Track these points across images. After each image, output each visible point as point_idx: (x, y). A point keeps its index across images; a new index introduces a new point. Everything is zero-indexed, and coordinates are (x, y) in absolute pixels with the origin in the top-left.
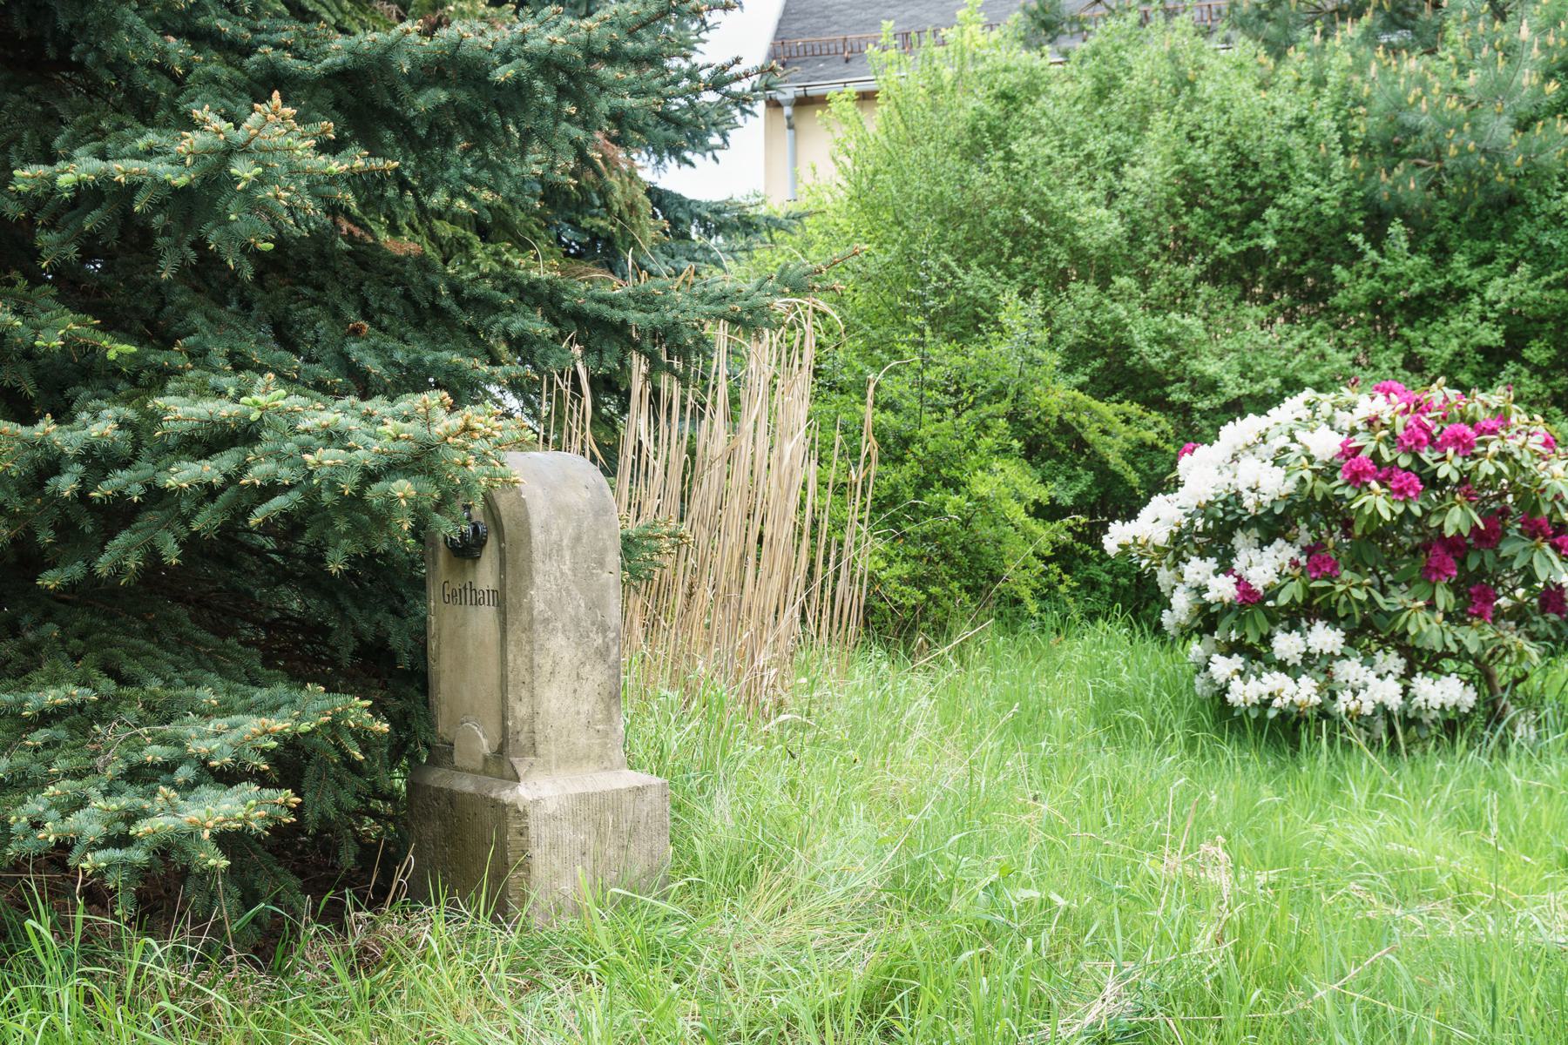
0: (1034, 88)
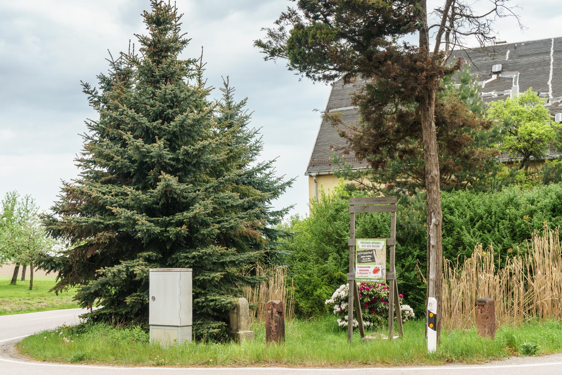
0: (343, 207)
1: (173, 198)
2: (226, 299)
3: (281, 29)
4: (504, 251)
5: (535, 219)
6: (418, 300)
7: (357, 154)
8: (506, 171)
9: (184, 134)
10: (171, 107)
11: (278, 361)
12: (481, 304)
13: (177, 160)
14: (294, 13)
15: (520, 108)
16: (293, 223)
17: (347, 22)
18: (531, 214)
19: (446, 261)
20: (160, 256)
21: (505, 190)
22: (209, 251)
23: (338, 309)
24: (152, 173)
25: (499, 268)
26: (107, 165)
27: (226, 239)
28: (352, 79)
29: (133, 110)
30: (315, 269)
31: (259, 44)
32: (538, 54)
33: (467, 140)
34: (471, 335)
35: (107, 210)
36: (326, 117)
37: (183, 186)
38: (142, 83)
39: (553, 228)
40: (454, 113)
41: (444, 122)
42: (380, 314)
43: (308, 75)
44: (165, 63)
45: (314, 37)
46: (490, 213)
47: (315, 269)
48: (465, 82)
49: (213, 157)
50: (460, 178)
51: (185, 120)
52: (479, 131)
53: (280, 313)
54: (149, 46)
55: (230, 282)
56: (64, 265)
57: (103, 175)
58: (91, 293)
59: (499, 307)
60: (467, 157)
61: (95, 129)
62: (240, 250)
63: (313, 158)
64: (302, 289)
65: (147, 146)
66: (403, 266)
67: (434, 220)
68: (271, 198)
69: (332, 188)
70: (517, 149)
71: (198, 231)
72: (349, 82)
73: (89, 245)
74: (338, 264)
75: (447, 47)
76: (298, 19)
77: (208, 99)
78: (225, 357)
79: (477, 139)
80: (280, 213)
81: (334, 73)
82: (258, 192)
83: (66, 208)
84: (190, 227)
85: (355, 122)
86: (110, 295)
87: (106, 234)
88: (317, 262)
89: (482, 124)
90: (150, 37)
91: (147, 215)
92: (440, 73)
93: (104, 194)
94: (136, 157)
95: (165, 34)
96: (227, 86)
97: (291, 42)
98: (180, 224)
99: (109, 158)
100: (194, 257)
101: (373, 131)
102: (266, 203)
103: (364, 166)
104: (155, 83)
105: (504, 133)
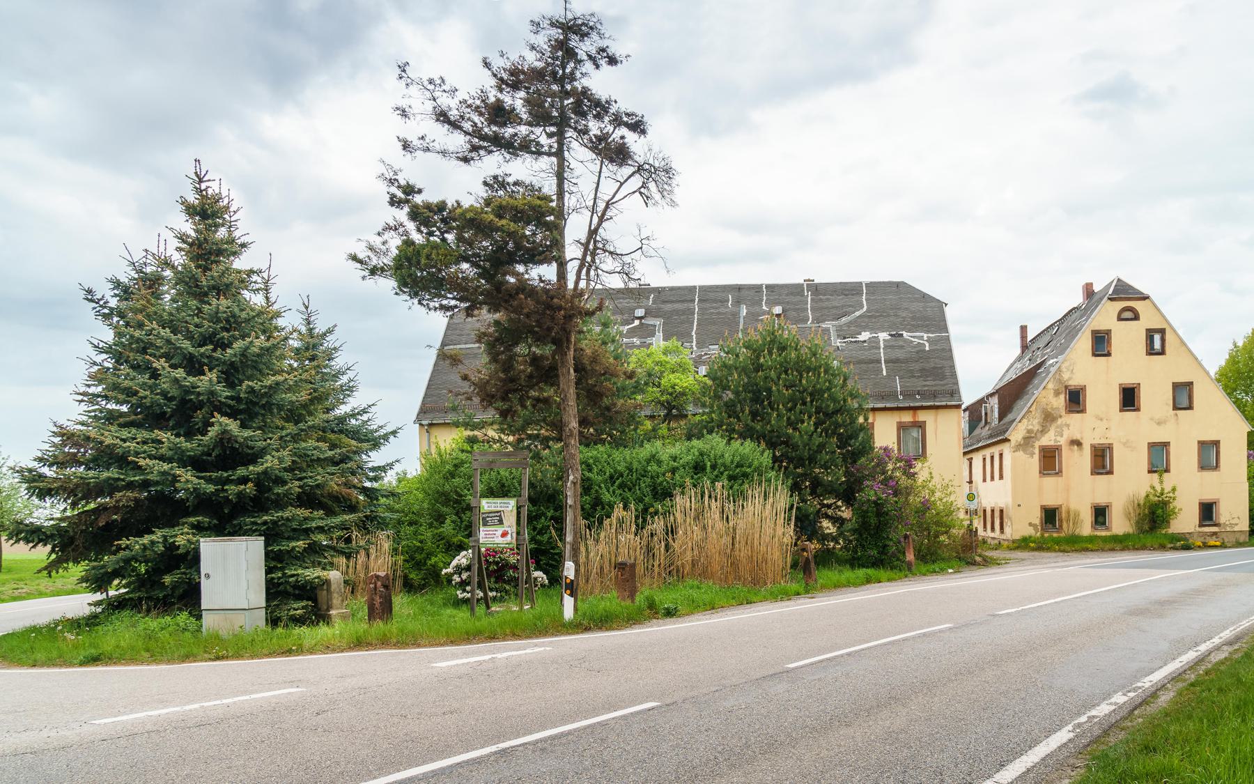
0: (463, 462)
1: (233, 448)
2: (312, 573)
3: (384, 243)
4: (645, 510)
5: (677, 477)
6: (551, 565)
7: (482, 400)
8: (648, 425)
9: (247, 366)
10: (228, 330)
11: (384, 642)
12: (621, 566)
13: (238, 399)
14: (401, 225)
15: (664, 358)
16: (399, 481)
17: (470, 243)
18: (674, 471)
19: (584, 522)
20: (215, 521)
21: (647, 446)
22: (286, 514)
23: (458, 580)
24: (199, 415)
25: (640, 528)
26: (128, 402)
27: (309, 499)
28: (476, 312)
29: (168, 330)
30: (428, 534)
31: (354, 258)
32: (683, 301)
33: (609, 390)
34: (611, 601)
35: (129, 463)
36: (442, 356)
37: (247, 433)
38: (180, 294)
39: (695, 486)
40: (595, 359)
41: (584, 369)
42: (508, 582)
43: (420, 303)
44: (215, 271)
45: (428, 257)
46: (631, 470)
47: (428, 534)
48: (605, 325)
49: (289, 396)
50: (599, 432)
51: (248, 348)
52: (621, 381)
53: (386, 587)
54: (191, 245)
55: (316, 552)
56: (61, 536)
57: (122, 414)
58: (107, 573)
59: (640, 570)
60: (608, 409)
61: (106, 353)
62: (330, 513)
63: (423, 403)
64: (412, 558)
65: (191, 379)
66: (534, 529)
67: (571, 478)
68: (371, 450)
69: (449, 440)
70: (659, 402)
71: (270, 489)
72: (472, 316)
73: (101, 509)
74: (457, 527)
75: (588, 284)
76: (406, 233)
77: (280, 322)
78: (313, 642)
79: (618, 390)
80: (383, 469)
81: (453, 303)
82: (354, 443)
83: (61, 458)
84: (258, 484)
85: (479, 363)
86: (138, 575)
87: (129, 494)
88: (431, 526)
89: (625, 373)
90: (193, 234)
91: (194, 468)
92: (580, 313)
93: (124, 441)
94: (174, 392)
95: (216, 231)
96: (307, 308)
97: (398, 259)
98: (244, 480)
99: (131, 393)
100: (265, 523)
101: (502, 375)
102: (364, 456)
103: (490, 414)
104: (202, 296)
105: (646, 384)
